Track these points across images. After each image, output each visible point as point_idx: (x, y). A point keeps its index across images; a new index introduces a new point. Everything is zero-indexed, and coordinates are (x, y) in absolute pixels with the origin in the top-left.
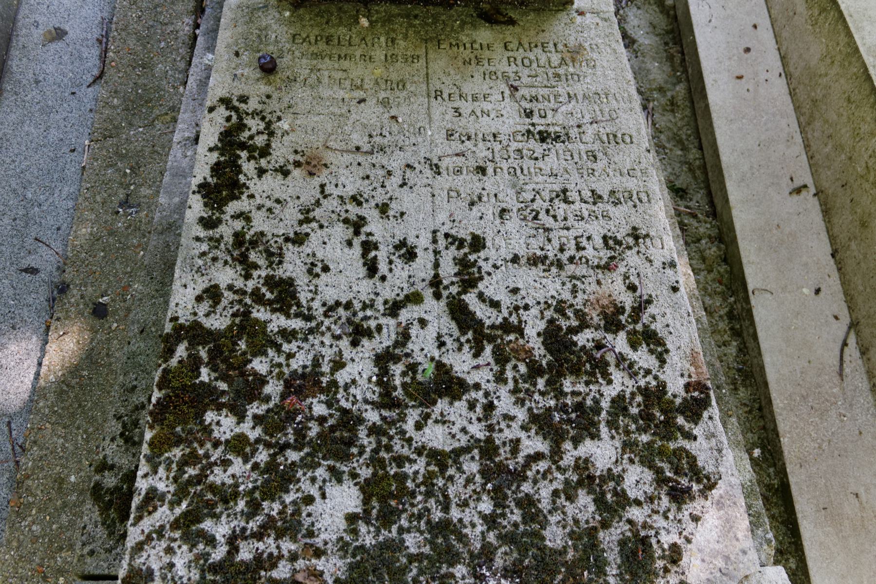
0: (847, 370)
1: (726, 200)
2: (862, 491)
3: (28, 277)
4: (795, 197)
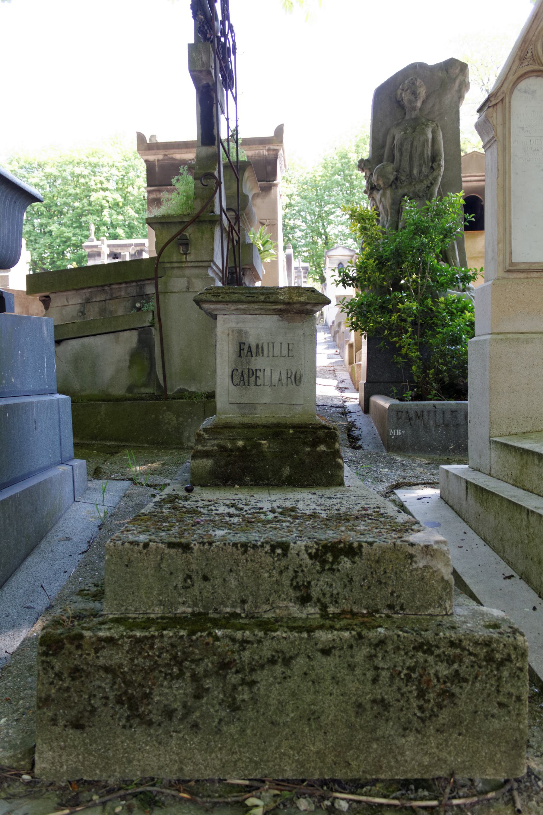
4: (508, 580)
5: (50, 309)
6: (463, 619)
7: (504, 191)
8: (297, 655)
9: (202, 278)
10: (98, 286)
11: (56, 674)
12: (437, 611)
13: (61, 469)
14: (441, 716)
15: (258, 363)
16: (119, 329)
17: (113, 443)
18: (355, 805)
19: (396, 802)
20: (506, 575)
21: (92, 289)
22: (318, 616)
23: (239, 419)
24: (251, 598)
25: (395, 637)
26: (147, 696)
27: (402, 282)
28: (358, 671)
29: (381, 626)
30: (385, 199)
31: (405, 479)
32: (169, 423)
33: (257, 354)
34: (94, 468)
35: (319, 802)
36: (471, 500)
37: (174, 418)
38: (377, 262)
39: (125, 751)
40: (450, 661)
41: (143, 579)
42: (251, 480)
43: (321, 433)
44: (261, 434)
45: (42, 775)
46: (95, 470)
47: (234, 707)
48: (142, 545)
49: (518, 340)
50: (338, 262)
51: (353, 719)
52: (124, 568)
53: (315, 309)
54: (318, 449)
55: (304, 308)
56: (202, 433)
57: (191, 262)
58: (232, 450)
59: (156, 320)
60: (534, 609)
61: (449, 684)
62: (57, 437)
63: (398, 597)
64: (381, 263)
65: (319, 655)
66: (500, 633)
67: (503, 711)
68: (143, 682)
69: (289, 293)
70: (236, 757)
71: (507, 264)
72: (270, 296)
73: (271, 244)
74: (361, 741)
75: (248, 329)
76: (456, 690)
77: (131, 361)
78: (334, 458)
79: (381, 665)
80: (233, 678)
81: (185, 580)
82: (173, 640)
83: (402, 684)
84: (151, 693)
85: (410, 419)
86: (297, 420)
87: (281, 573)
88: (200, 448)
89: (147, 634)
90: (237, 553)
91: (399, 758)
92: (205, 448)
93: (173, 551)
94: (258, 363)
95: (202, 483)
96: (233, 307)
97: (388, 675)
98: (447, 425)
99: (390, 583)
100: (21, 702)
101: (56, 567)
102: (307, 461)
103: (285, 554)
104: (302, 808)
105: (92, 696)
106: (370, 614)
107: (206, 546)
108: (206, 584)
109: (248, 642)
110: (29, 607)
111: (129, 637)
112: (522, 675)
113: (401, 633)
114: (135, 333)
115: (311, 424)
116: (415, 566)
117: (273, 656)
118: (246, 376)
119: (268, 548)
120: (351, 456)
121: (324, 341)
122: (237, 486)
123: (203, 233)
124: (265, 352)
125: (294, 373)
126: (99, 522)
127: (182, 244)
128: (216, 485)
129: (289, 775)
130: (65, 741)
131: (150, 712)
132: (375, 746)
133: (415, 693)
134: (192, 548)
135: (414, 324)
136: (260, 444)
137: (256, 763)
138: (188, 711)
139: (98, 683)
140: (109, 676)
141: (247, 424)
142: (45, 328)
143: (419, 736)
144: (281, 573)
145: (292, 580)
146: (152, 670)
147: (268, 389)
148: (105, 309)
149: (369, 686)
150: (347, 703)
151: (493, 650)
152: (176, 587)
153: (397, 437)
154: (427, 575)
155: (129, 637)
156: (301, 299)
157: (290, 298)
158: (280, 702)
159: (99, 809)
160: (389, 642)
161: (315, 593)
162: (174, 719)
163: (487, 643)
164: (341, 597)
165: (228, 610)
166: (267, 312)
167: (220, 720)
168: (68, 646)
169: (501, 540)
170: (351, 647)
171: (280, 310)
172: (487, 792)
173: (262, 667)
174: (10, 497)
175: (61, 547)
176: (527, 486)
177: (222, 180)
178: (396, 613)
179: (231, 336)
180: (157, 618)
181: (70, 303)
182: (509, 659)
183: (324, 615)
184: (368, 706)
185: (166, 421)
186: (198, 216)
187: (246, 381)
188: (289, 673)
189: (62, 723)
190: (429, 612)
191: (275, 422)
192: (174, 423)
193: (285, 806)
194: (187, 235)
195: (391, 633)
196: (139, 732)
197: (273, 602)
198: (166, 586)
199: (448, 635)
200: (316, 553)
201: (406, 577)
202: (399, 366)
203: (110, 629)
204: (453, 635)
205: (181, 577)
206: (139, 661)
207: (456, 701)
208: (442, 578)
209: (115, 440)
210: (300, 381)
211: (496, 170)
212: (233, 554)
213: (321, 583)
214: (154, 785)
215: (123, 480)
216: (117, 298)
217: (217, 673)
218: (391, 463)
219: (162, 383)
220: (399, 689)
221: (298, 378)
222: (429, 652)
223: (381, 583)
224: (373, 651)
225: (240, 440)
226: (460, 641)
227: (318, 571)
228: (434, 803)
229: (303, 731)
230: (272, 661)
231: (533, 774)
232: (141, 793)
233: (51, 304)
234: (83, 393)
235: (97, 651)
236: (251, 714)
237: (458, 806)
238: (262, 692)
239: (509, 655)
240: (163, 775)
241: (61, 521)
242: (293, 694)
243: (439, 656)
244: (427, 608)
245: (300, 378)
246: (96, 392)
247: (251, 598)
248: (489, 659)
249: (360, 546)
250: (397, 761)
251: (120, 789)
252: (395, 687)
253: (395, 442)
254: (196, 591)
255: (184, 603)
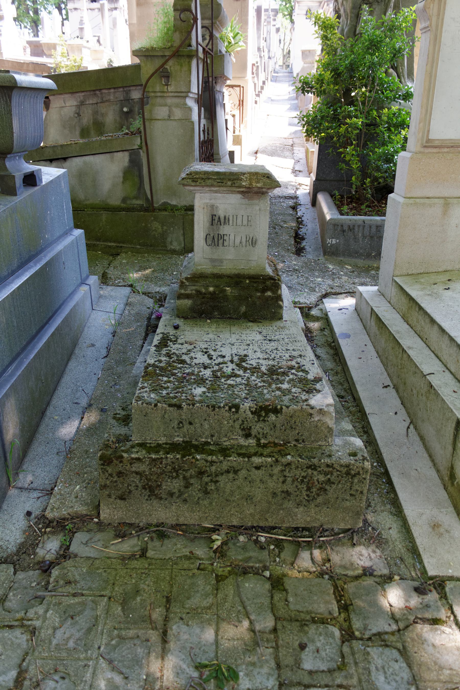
0: (410, 435)
1: (357, 391)
2: (419, 469)
3: (76, 405)
4: (385, 389)
5: (50, 109)
6: (337, 448)
7: (431, 77)
8: (242, 469)
9: (181, 108)
10: (90, 91)
11: (109, 475)
12: (324, 443)
13: (84, 288)
14: (318, 500)
15: (225, 230)
16: (114, 150)
17: (113, 244)
18: (269, 539)
19: (290, 538)
20: (385, 385)
21: (85, 93)
22: (255, 444)
23: (210, 270)
24: (216, 434)
25: (297, 462)
26: (159, 486)
27: (353, 94)
28: (275, 478)
29: (289, 454)
30: (347, 2)
31: (332, 288)
32: (155, 230)
33: (225, 223)
34: (102, 272)
35: (250, 537)
36: (373, 323)
37: (160, 227)
38: (333, 74)
39: (148, 510)
40: (326, 474)
41: (154, 423)
42: (219, 315)
43: (268, 283)
44: (226, 283)
45: (104, 520)
46: (103, 274)
47: (206, 492)
48: (153, 405)
49: (424, 204)
50: (306, 8)
51: (271, 500)
52: (143, 417)
53: (269, 191)
54: (266, 294)
55: (261, 190)
56: (184, 281)
57: (172, 92)
58: (205, 294)
59: (144, 144)
60: (396, 413)
61: (324, 485)
62: (78, 266)
63: (302, 435)
64: (337, 74)
65: (254, 469)
66: (356, 460)
67: (352, 498)
68: (157, 480)
69: (250, 179)
70: (207, 515)
71: (424, 141)
72: (236, 182)
73: (241, 36)
74: (274, 509)
75: (218, 205)
76: (328, 487)
77: (124, 177)
78: (277, 301)
79: (288, 475)
80: (206, 479)
81: (179, 424)
82: (173, 460)
83: (298, 484)
84: (161, 485)
85: (344, 231)
86: (252, 272)
87: (234, 421)
88: (183, 291)
89: (158, 456)
90: (209, 411)
91: (294, 517)
92: (186, 292)
93: (171, 409)
94: (225, 230)
95: (184, 316)
96: (207, 189)
97: (291, 479)
98: (372, 237)
99: (298, 428)
100: (86, 475)
101: (88, 370)
102: (258, 303)
103: (237, 412)
104: (241, 540)
105: (129, 485)
106: (285, 444)
107: (191, 407)
108: (191, 426)
109: (214, 462)
110: (76, 403)
111: (149, 458)
112: (365, 481)
113: (300, 459)
114: (127, 154)
115: (262, 275)
116: (312, 419)
117: (228, 469)
118: (216, 239)
119: (227, 408)
120: (295, 265)
121: (287, 97)
122: (209, 321)
123: (181, 66)
124: (231, 222)
125: (251, 238)
126: (111, 329)
127: (164, 77)
128: (195, 318)
129: (235, 523)
130: (115, 505)
131: (161, 493)
132: (282, 512)
133: (305, 488)
134: (183, 408)
135: (358, 137)
136: (225, 290)
137: (217, 518)
138: (181, 493)
139: (132, 479)
140: (138, 476)
141: (217, 274)
142: (63, 182)
143: (306, 508)
144: (234, 421)
145: (241, 425)
146: (161, 474)
147: (232, 249)
148: (97, 112)
149: (280, 485)
150: (268, 492)
151: (350, 469)
152: (173, 427)
153: (332, 245)
154: (319, 424)
155: (149, 458)
156: (259, 185)
157: (251, 184)
158: (231, 491)
159: (136, 538)
160: (293, 464)
161: (254, 432)
162: (174, 497)
163: (347, 466)
164: (269, 435)
165: (203, 440)
166: (233, 192)
167: (199, 498)
168: (115, 461)
169: (387, 358)
170: (272, 466)
171: (243, 191)
172: (339, 534)
173: (222, 474)
174: (56, 330)
175: (89, 352)
176: (410, 323)
177: (199, 16)
178: (300, 444)
179: (205, 210)
180: (163, 444)
181: (67, 105)
182: (359, 473)
183: (259, 445)
184: (279, 494)
185: (154, 229)
186: (178, 51)
187: (216, 243)
188: (236, 477)
189: (114, 497)
190: (319, 443)
191: (237, 272)
192: (160, 230)
193: (232, 538)
194: (168, 68)
195: (294, 460)
196: (155, 502)
197: (229, 436)
198: (168, 427)
199: (326, 461)
200: (256, 411)
201: (307, 425)
202: (343, 172)
203: (137, 452)
204: (329, 461)
205: (176, 422)
206: (154, 469)
207: (327, 492)
208: (328, 426)
209: (114, 242)
210: (255, 244)
211: (427, 57)
212: (206, 411)
213: (257, 427)
214: (163, 527)
215: (125, 286)
216: (107, 101)
217: (197, 476)
218: (324, 271)
219: (149, 197)
220: (297, 486)
221: (254, 241)
222: (315, 469)
223: (292, 428)
224: (284, 468)
225: (211, 286)
226: (333, 464)
227: (256, 421)
228: (311, 539)
229: (243, 504)
230: (228, 472)
231: (367, 522)
232: (157, 530)
233: (51, 105)
234: (88, 202)
235: (131, 464)
236: (215, 496)
237: (323, 541)
238: (222, 486)
239: (359, 472)
240: (168, 521)
241: (86, 329)
242: (239, 487)
243: (320, 471)
244: (317, 442)
245: (256, 242)
246: (97, 202)
247: (216, 434)
248: (348, 473)
249: (282, 408)
250: (293, 519)
251: (147, 528)
252: (294, 485)
253: (331, 249)
254: (185, 429)
255: (178, 436)
